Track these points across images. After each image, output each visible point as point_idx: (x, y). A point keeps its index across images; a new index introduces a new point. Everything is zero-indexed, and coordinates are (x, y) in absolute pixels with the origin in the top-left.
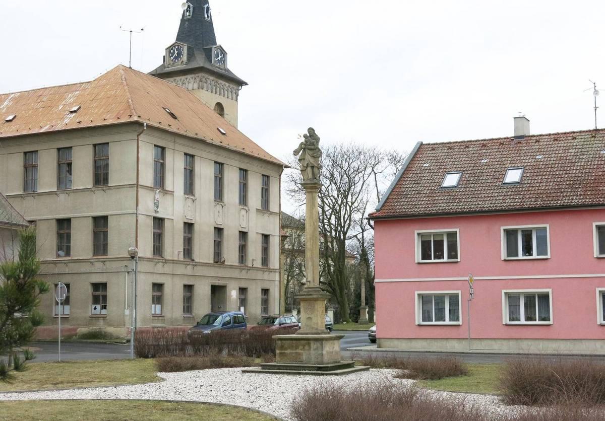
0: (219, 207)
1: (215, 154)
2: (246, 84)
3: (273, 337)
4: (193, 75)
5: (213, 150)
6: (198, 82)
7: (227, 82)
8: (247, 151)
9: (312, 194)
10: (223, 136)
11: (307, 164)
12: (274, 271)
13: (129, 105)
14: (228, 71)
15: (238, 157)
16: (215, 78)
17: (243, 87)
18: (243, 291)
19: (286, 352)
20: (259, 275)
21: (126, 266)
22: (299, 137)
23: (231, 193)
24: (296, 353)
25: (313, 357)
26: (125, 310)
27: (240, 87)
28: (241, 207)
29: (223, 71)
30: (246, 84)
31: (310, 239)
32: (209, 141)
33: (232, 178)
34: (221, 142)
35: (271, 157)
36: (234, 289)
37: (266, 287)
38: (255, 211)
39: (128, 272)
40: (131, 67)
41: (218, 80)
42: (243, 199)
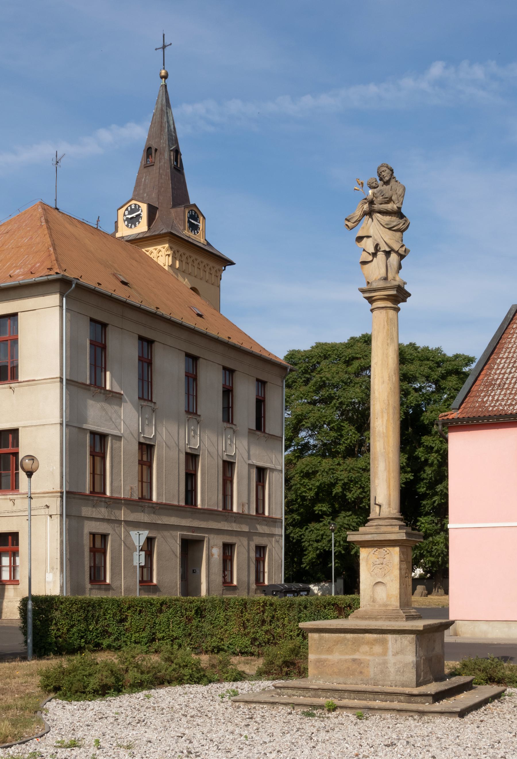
2: (232, 263)
9: (387, 313)
11: (377, 247)
12: (272, 521)
13: (49, 255)
17: (227, 267)
19: (330, 657)
21: (47, 506)
23: (210, 402)
24: (354, 660)
25: (392, 670)
26: (47, 575)
28: (225, 424)
30: (232, 263)
31: (382, 412)
33: (211, 380)
35: (270, 354)
39: (51, 516)
40: (58, 207)
42: (228, 414)
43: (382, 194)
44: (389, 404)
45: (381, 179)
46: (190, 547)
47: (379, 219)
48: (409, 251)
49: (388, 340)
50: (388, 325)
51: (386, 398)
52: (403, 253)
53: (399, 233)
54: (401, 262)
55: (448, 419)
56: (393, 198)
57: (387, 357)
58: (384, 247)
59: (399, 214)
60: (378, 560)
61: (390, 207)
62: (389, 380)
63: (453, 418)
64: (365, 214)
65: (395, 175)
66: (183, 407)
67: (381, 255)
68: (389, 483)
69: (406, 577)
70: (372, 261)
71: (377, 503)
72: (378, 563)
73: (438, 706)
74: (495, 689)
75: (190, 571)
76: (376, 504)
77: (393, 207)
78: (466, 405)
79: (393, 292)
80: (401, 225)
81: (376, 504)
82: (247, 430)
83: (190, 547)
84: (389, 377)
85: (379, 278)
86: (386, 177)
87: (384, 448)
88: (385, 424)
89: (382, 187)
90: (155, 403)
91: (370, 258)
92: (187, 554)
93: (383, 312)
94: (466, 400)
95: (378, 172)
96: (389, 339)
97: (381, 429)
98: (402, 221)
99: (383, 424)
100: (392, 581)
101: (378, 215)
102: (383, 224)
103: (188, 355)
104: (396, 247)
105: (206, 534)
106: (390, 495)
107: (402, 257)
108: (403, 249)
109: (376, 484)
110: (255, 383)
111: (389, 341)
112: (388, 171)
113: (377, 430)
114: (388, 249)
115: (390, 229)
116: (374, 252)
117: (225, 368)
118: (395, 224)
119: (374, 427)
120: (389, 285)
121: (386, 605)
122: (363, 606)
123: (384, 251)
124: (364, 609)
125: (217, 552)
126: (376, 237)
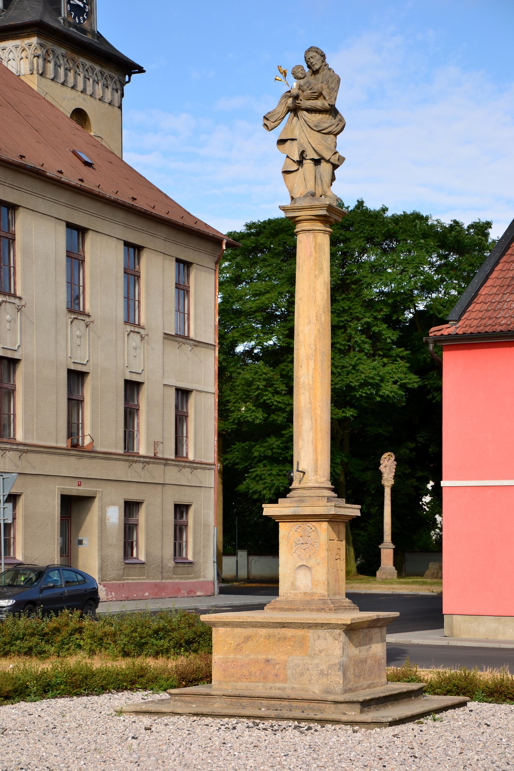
0: (79, 327)
1: (67, 206)
2: (141, 70)
3: (204, 618)
4: (18, 42)
5: (65, 197)
6: (31, 57)
7: (96, 63)
8: (142, 204)
9: (315, 237)
10: (86, 169)
11: (302, 154)
12: (197, 465)
14: (99, 36)
15: (120, 216)
16: (69, 52)
17: (133, 76)
18: (131, 507)
20: (172, 474)
22: (280, 77)
27: (127, 77)
29: (89, 37)
30: (141, 70)
32: (51, 173)
34: (81, 180)
35: (197, 221)
36: (113, 504)
37: (183, 500)
38: (161, 339)
41: (76, 57)
43: (310, 88)
44: (316, 350)
45: (309, 67)
46: (73, 507)
47: (306, 119)
48: (344, 159)
49: (315, 270)
50: (315, 252)
51: (313, 342)
52: (337, 163)
53: (332, 136)
54: (335, 171)
55: (442, 335)
56: (324, 93)
57: (314, 292)
58: (311, 154)
59: (332, 111)
60: (301, 538)
61: (319, 103)
62: (317, 320)
63: (449, 334)
64: (289, 110)
65: (327, 61)
66: (63, 305)
67: (308, 165)
68: (316, 446)
69: (337, 560)
70: (298, 169)
71: (300, 470)
72: (301, 542)
73: (370, 716)
74: (461, 698)
75: (74, 542)
76: (298, 471)
77: (323, 104)
78: (470, 315)
79: (323, 212)
80: (334, 126)
81: (298, 471)
82: (161, 336)
83: (73, 507)
84: (316, 316)
85: (305, 193)
86: (316, 65)
87: (310, 403)
88: (311, 373)
89: (310, 79)
90: (20, 298)
91: (295, 167)
92: (70, 517)
93: (311, 235)
94: (470, 308)
95: (305, 57)
96: (317, 270)
97: (306, 380)
98: (335, 121)
99: (308, 373)
100: (318, 564)
101: (305, 113)
102: (312, 126)
103: (70, 226)
104: (327, 155)
105: (99, 488)
106: (317, 460)
107: (335, 167)
108: (336, 157)
109: (300, 447)
110: (174, 264)
111: (317, 272)
112: (318, 57)
113: (301, 380)
114: (316, 157)
115: (319, 131)
116: (298, 159)
117: (127, 244)
118: (326, 125)
119: (297, 377)
120: (318, 203)
121: (312, 594)
122: (282, 595)
123: (312, 160)
124: (284, 598)
125: (114, 515)
126: (302, 141)
